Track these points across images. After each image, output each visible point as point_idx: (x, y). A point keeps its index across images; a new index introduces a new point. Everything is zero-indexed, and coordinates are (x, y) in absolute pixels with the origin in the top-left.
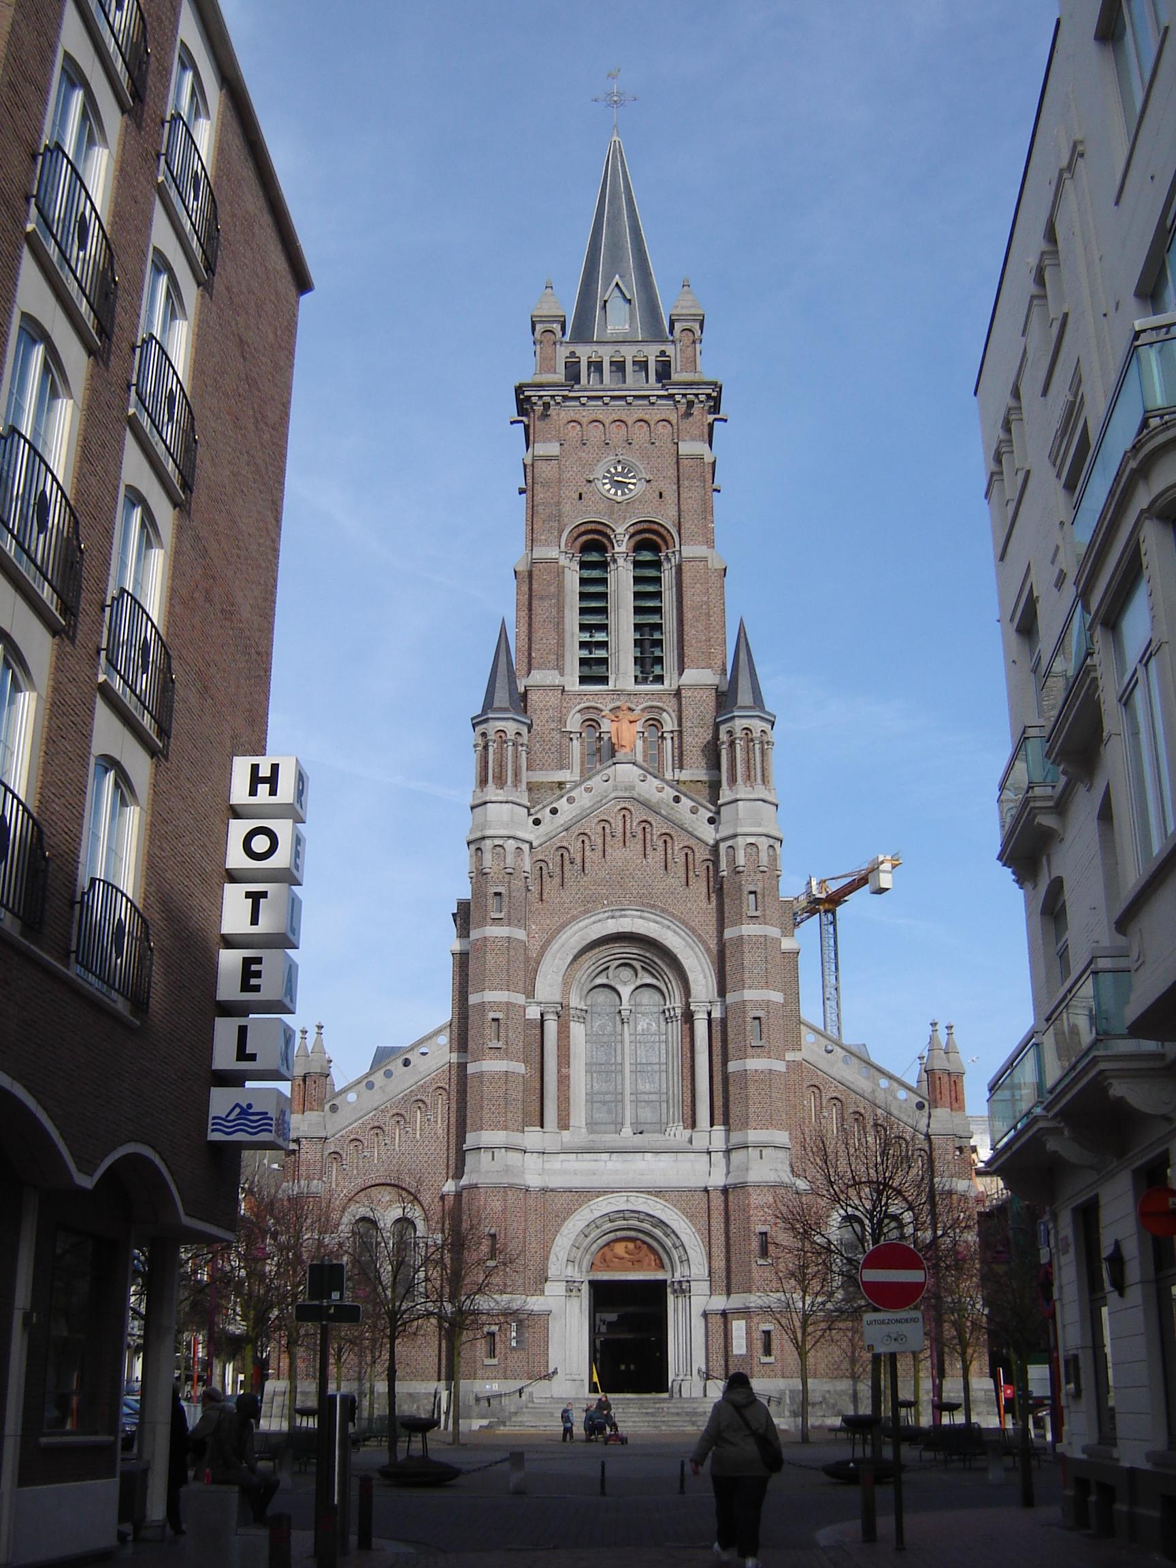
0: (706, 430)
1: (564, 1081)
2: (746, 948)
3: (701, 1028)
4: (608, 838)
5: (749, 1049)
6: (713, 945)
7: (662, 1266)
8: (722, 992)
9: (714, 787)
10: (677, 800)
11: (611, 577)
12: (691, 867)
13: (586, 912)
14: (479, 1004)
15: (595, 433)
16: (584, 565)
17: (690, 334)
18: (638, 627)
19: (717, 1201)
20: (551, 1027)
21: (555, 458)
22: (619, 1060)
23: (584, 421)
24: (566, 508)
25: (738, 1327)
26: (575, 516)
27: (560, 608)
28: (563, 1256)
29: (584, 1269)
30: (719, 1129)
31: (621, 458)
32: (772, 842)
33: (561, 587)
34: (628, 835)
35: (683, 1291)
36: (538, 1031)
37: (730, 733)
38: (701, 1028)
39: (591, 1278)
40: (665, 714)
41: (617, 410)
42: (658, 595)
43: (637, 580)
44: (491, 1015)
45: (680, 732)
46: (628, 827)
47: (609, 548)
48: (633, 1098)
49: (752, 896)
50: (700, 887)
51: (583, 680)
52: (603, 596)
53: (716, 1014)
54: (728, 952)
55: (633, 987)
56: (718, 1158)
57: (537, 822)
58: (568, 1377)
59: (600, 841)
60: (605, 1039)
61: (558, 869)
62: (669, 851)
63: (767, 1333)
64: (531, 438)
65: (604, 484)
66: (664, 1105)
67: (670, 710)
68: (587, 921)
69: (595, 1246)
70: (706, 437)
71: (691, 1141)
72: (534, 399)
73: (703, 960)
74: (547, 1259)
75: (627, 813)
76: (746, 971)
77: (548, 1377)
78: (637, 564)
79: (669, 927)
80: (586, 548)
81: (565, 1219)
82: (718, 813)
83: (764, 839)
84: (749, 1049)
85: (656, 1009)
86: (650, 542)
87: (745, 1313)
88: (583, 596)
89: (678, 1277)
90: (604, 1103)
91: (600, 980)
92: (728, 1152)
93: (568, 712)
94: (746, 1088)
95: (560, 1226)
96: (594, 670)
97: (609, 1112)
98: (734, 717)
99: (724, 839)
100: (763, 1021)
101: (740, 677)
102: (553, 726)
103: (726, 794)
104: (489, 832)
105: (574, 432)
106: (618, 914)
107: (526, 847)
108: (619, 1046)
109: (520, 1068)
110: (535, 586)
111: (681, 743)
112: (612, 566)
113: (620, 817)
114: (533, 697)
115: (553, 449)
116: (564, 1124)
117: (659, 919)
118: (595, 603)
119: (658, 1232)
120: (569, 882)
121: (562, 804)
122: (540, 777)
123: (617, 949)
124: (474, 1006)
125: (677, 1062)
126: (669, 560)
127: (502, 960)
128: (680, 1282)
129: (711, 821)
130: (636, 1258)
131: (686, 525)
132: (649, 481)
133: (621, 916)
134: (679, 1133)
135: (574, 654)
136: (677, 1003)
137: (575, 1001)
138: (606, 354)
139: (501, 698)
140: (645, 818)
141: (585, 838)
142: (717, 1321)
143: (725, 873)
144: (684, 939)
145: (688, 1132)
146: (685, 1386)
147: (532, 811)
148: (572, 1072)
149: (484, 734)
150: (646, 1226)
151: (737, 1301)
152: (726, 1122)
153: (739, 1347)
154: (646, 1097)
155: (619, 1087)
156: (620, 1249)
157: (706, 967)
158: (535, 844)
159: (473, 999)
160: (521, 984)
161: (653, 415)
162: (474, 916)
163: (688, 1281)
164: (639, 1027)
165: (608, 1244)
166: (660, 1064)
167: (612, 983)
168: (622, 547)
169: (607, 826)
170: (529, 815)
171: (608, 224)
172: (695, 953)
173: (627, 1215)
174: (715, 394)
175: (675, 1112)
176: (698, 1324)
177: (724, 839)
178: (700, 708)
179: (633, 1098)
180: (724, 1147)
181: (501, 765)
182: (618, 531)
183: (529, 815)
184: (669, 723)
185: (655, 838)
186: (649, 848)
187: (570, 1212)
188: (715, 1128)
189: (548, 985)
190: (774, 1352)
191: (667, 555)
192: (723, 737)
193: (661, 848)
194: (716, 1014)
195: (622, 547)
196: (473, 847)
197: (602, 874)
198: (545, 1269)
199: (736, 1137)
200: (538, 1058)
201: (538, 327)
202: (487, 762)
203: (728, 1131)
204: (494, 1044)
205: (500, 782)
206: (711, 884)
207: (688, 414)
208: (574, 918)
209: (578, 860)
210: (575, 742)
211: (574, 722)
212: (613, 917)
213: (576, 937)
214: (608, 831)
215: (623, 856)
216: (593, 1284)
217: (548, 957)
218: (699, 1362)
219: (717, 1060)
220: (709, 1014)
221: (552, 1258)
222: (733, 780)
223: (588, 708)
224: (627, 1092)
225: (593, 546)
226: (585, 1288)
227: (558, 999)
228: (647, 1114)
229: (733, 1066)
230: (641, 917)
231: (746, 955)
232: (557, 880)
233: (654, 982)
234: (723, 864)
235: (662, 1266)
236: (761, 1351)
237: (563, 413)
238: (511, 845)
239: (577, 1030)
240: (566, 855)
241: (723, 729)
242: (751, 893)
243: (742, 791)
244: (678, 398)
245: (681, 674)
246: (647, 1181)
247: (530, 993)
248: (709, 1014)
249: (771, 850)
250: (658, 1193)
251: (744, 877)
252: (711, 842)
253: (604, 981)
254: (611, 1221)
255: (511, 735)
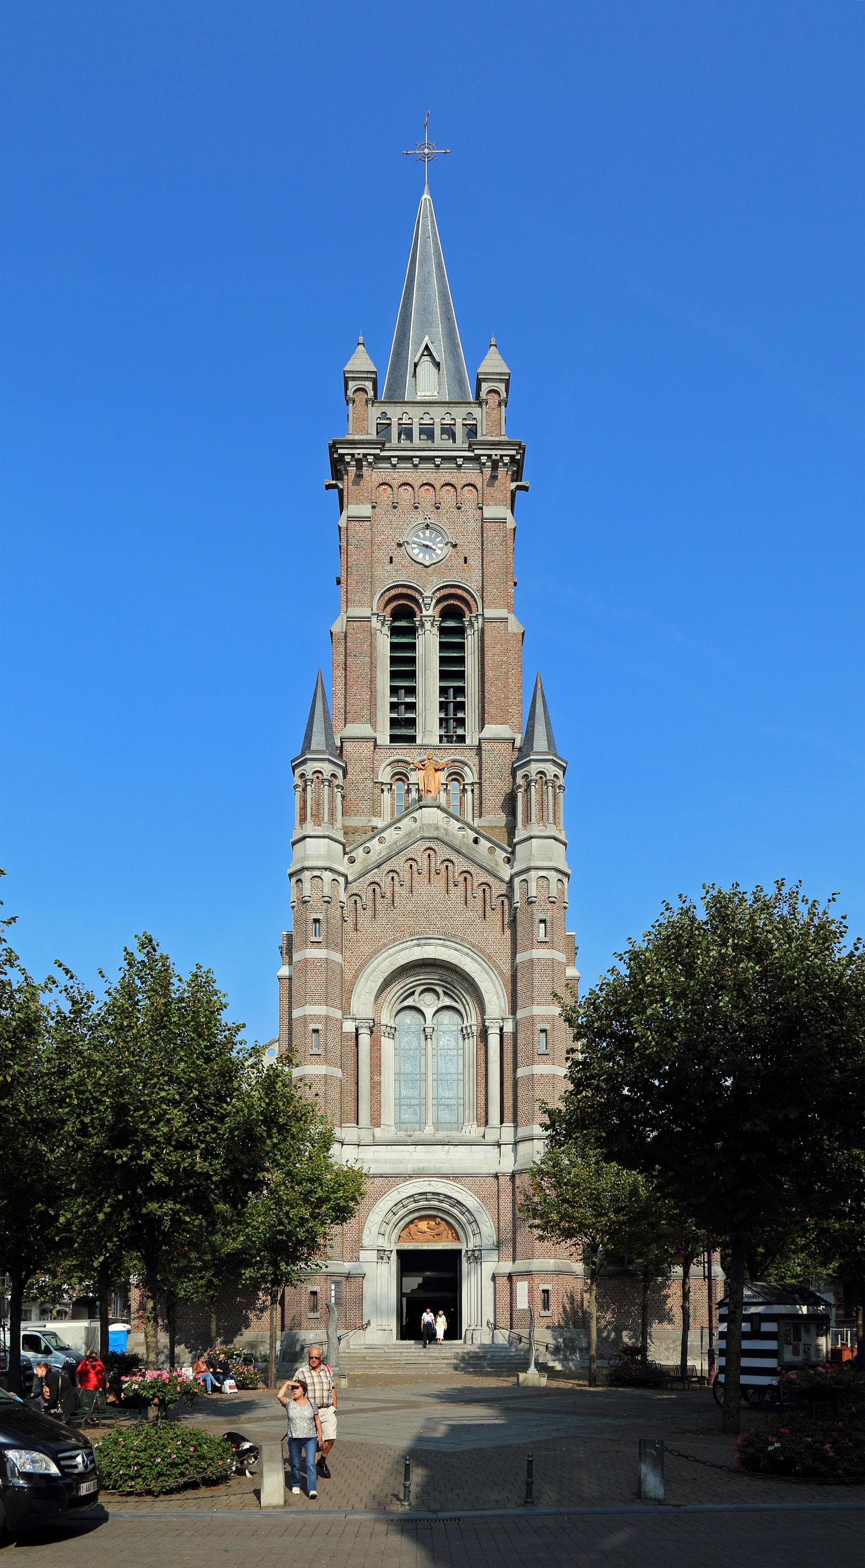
0: (509, 495)
1: (376, 1086)
2: (537, 970)
3: (494, 1041)
4: (415, 875)
5: (536, 1057)
6: (507, 969)
7: (457, 1238)
8: (514, 1011)
9: (511, 829)
10: (476, 841)
11: (420, 642)
12: (488, 902)
13: (395, 940)
14: (301, 1017)
15: (406, 495)
16: (394, 631)
17: (496, 396)
18: (443, 691)
19: (505, 1182)
20: (365, 1040)
21: (367, 519)
22: (423, 1070)
23: (395, 484)
24: (379, 572)
25: (522, 1287)
26: (388, 577)
27: (373, 666)
28: (375, 1229)
29: (392, 1241)
30: (508, 1124)
31: (428, 521)
32: (560, 877)
33: (372, 646)
34: (433, 871)
35: (476, 1258)
36: (353, 1042)
37: (526, 776)
38: (494, 1041)
39: (399, 1248)
40: (466, 768)
41: (427, 473)
42: (461, 661)
43: (443, 646)
44: (312, 1026)
45: (480, 784)
46: (433, 865)
47: (418, 612)
48: (435, 1102)
49: (542, 925)
50: (495, 918)
51: (394, 738)
52: (412, 661)
53: (509, 1028)
54: (519, 974)
55: (435, 1009)
56: (507, 1150)
57: (352, 861)
58: (379, 1327)
59: (407, 877)
60: (411, 1053)
61: (370, 903)
62: (469, 888)
63: (546, 1292)
64: (345, 500)
65: (413, 549)
66: (461, 1108)
67: (471, 765)
68: (397, 948)
69: (402, 1222)
70: (509, 502)
71: (484, 1136)
72: (348, 459)
73: (497, 983)
74: (362, 1232)
75: (431, 853)
76: (535, 990)
77: (363, 1327)
78: (443, 631)
79: (467, 954)
80: (397, 614)
81: (377, 1199)
82: (513, 853)
83: (553, 873)
84: (536, 1057)
85: (454, 1028)
86: (454, 611)
87: (527, 1274)
88: (394, 661)
89: (471, 1246)
90: (410, 1106)
91: (409, 1002)
92: (515, 1144)
93: (380, 765)
94: (533, 1090)
95: (373, 1205)
96: (403, 729)
97: (414, 1113)
98: (530, 761)
99: (518, 874)
100: (549, 1032)
101: (536, 726)
102: (366, 775)
103: (521, 833)
104: (308, 864)
105: (385, 495)
106: (423, 941)
107: (341, 880)
108: (423, 1060)
109: (338, 1073)
110: (349, 644)
111: (481, 794)
112: (420, 631)
113: (426, 856)
114: (348, 746)
115: (365, 510)
116: (376, 1121)
117: (459, 947)
118: (403, 668)
119: (454, 1211)
120: (380, 915)
121: (374, 844)
122: (355, 821)
123: (424, 977)
124: (338, 1433)
125: (473, 1072)
126: (472, 624)
127: (322, 978)
128: (473, 1251)
129: (509, 861)
130: (437, 1231)
131: (489, 588)
132: (455, 546)
133: (425, 944)
134: (473, 1131)
135: (385, 715)
136: (473, 1020)
137: (386, 1018)
138: (415, 417)
139: (318, 741)
140: (447, 857)
141: (395, 875)
142: (503, 1282)
143: (518, 905)
144: (480, 964)
145: (482, 1129)
146: (477, 1334)
147: (348, 850)
148: (382, 1079)
149: (302, 776)
150: (445, 1206)
151: (521, 1265)
152: (515, 1121)
153: (522, 1303)
154: (446, 1102)
155: (423, 1093)
156: (423, 1225)
157: (499, 988)
158: (350, 879)
159: (296, 1014)
160: (338, 1001)
161: (459, 478)
162: (297, 941)
163: (480, 1250)
164: (441, 1043)
165: (412, 1222)
166: (458, 1074)
167: (418, 1005)
168: (429, 612)
169: (414, 864)
170: (345, 853)
171: (418, 288)
172: (490, 977)
173: (429, 1196)
174: (518, 457)
175: (470, 1113)
176: (488, 1285)
177: (518, 874)
178: (499, 758)
179: (435, 1102)
180: (512, 1140)
181: (318, 803)
182: (425, 594)
183: (345, 853)
184: (470, 777)
185: (456, 874)
186: (451, 885)
187: (381, 1194)
188: (504, 1125)
189: (362, 1002)
190: (551, 1308)
191: (470, 621)
192: (520, 781)
193: (462, 885)
194: (509, 1028)
195: (429, 612)
196: (294, 880)
197: (410, 907)
198: (359, 1240)
199: (523, 1132)
200: (353, 1066)
201: (351, 384)
202: (305, 802)
203: (516, 1127)
204: (315, 1051)
205: (317, 819)
206: (507, 913)
207: (494, 478)
208: (385, 945)
209: (388, 894)
210: (386, 792)
211: (385, 775)
212: (418, 945)
213: (387, 962)
214: (415, 868)
215: (430, 891)
216: (400, 1253)
217: (362, 980)
218: (489, 1315)
219: (508, 1068)
220: (501, 1029)
221: (366, 1231)
222: (528, 819)
223: (398, 761)
224: (430, 1096)
225: (403, 612)
226: (394, 1256)
227: (371, 1017)
228: (446, 1116)
229: (521, 1072)
230: (443, 945)
231: (536, 975)
232: (369, 912)
233: (454, 1004)
234: (517, 897)
235: (457, 1238)
236: (541, 1306)
237: (374, 475)
238: (327, 876)
239: (387, 1044)
240: (378, 890)
241: (520, 774)
242: (543, 921)
243: (536, 829)
244: (484, 459)
245: (482, 727)
246: (446, 1168)
247: (346, 1009)
248: (501, 1029)
249: (560, 884)
250: (455, 1177)
251: (535, 907)
252: (507, 879)
253: (412, 1004)
254: (415, 1202)
255: (327, 775)
